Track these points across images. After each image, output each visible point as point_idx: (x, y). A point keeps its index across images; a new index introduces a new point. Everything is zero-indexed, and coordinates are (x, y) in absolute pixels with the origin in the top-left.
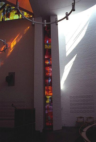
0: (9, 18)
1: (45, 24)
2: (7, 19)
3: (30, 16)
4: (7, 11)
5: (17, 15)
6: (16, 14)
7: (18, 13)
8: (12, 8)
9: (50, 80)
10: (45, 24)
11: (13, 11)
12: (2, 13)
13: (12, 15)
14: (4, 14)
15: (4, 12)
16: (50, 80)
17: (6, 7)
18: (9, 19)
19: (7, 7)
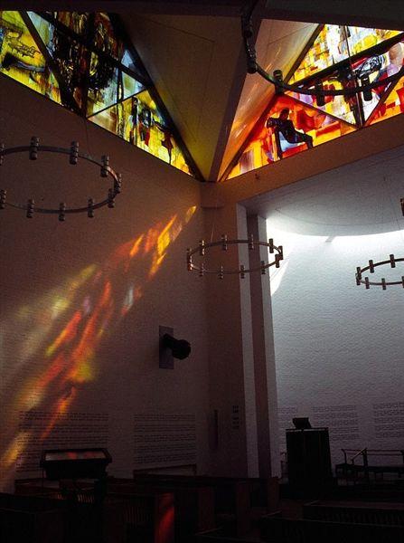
2: (141, 144)
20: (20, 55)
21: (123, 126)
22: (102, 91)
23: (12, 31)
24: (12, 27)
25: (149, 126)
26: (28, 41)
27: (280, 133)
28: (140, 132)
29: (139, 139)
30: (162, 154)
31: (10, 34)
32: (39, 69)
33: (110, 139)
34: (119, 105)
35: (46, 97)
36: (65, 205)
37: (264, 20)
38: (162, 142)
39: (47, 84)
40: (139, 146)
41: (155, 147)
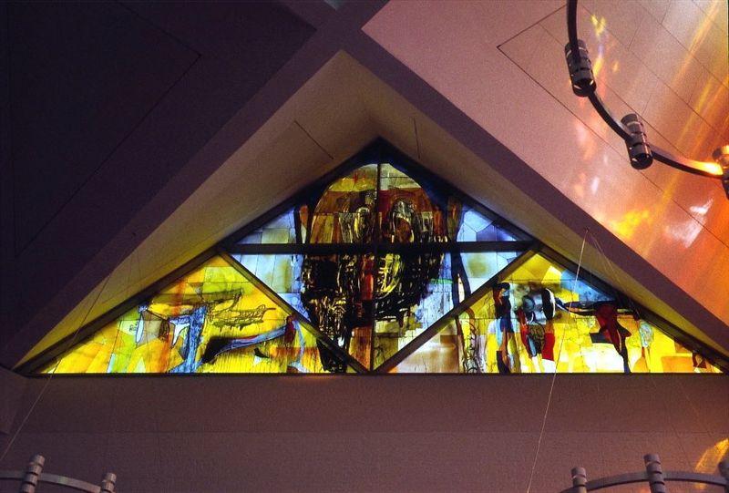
0: (549, 355)
1: (34, 479)
2: (532, 364)
3: (702, 366)
4: (524, 313)
5: (609, 349)
6: (596, 338)
7: (611, 334)
8: (558, 302)
9: (615, 68)
10: (34, 479)
11: (574, 320)
12: (494, 324)
13: (568, 345)
14: (506, 327)
15: (502, 310)
16: (713, 203)
17: (513, 286)
18: (546, 367)
19: (521, 287)
20: (236, 331)
21: (476, 349)
22: (415, 309)
23: (404, 276)
24: (220, 297)
25: (549, 318)
26: (259, 300)
27: (304, 242)
28: (526, 342)
29: (524, 357)
30: (604, 359)
31: (218, 308)
32: (272, 336)
33: (457, 386)
34: (464, 320)
35: (292, 372)
36: (583, 471)
37: (362, 29)
38: (592, 335)
39: (292, 350)
40: (525, 369)
41: (579, 351)
